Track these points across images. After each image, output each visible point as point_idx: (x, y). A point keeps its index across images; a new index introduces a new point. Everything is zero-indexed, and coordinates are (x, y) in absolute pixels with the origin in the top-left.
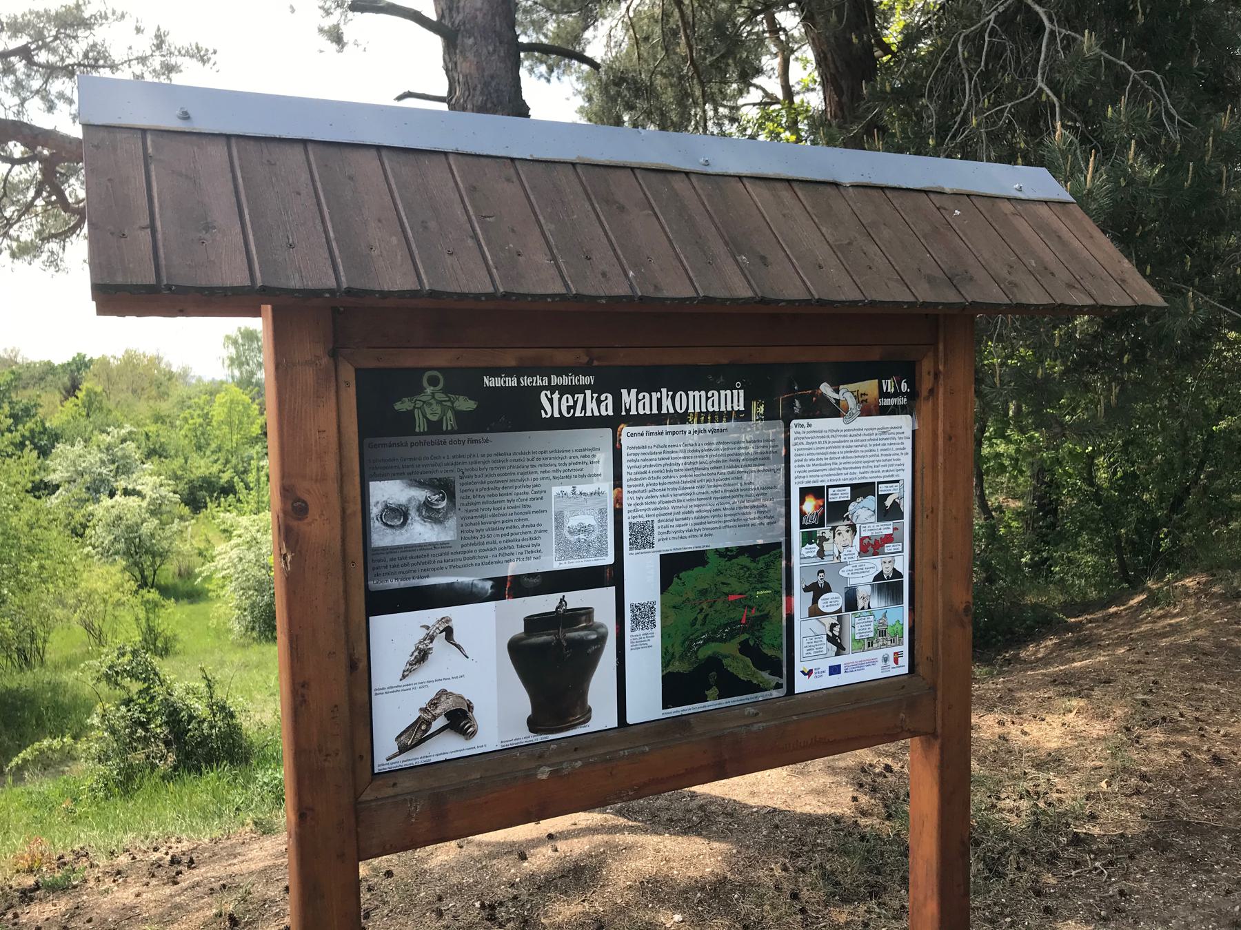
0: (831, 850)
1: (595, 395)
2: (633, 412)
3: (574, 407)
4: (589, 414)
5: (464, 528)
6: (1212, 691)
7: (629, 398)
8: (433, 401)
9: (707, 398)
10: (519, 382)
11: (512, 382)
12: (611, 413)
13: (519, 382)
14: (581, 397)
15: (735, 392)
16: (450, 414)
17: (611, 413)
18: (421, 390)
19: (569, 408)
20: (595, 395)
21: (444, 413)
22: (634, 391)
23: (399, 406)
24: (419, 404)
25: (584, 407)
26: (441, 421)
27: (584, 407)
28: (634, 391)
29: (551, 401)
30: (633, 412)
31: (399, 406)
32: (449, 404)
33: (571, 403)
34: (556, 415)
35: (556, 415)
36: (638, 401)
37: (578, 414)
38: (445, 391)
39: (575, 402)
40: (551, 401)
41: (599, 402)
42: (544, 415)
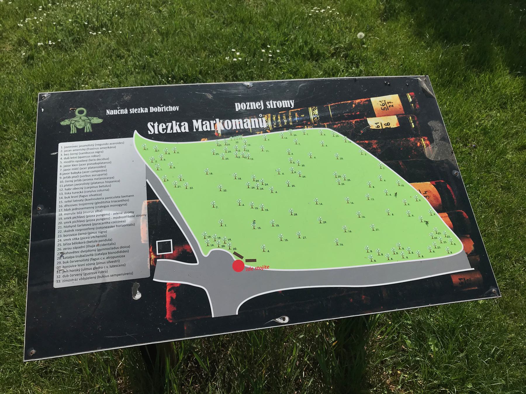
0: (6, 38)
1: (178, 123)
2: (200, 130)
3: (167, 129)
4: (175, 131)
5: (105, 172)
6: (43, 382)
7: (197, 124)
8: (80, 120)
9: (244, 123)
10: (129, 111)
11: (125, 112)
12: (187, 130)
13: (129, 111)
14: (170, 124)
15: (260, 119)
16: (89, 125)
17: (187, 130)
18: (74, 116)
19: (163, 130)
20: (178, 123)
21: (86, 125)
22: (200, 121)
23: (62, 123)
24: (73, 122)
25: (172, 128)
26: (84, 128)
27: (172, 128)
28: (200, 121)
29: (153, 127)
30: (200, 130)
31: (62, 123)
32: (89, 121)
33: (164, 127)
34: (157, 132)
35: (157, 132)
36: (202, 125)
37: (169, 131)
38: (87, 116)
39: (167, 127)
40: (153, 127)
41: (180, 126)
42: (149, 133)
